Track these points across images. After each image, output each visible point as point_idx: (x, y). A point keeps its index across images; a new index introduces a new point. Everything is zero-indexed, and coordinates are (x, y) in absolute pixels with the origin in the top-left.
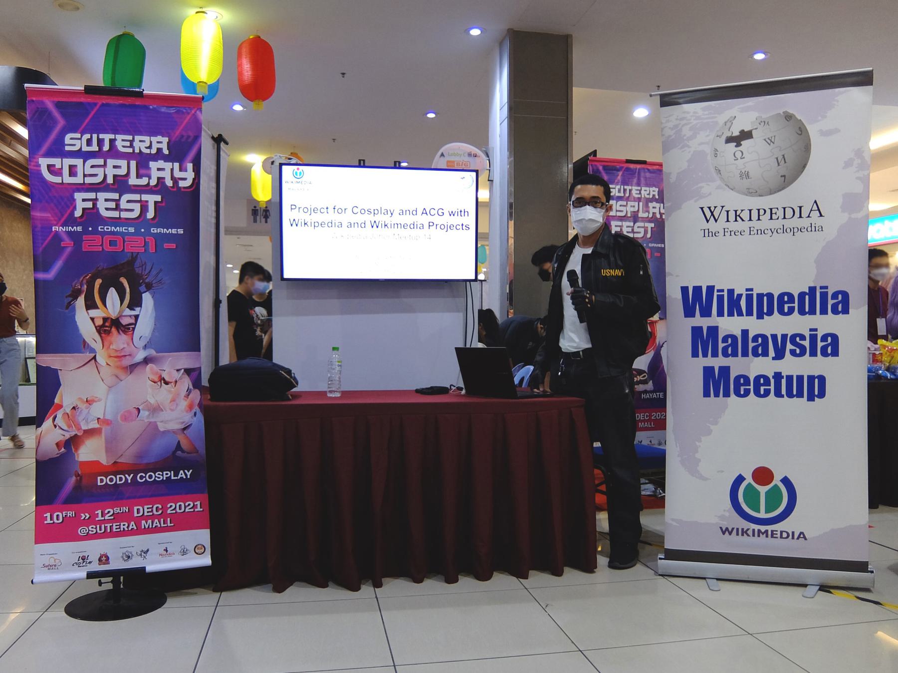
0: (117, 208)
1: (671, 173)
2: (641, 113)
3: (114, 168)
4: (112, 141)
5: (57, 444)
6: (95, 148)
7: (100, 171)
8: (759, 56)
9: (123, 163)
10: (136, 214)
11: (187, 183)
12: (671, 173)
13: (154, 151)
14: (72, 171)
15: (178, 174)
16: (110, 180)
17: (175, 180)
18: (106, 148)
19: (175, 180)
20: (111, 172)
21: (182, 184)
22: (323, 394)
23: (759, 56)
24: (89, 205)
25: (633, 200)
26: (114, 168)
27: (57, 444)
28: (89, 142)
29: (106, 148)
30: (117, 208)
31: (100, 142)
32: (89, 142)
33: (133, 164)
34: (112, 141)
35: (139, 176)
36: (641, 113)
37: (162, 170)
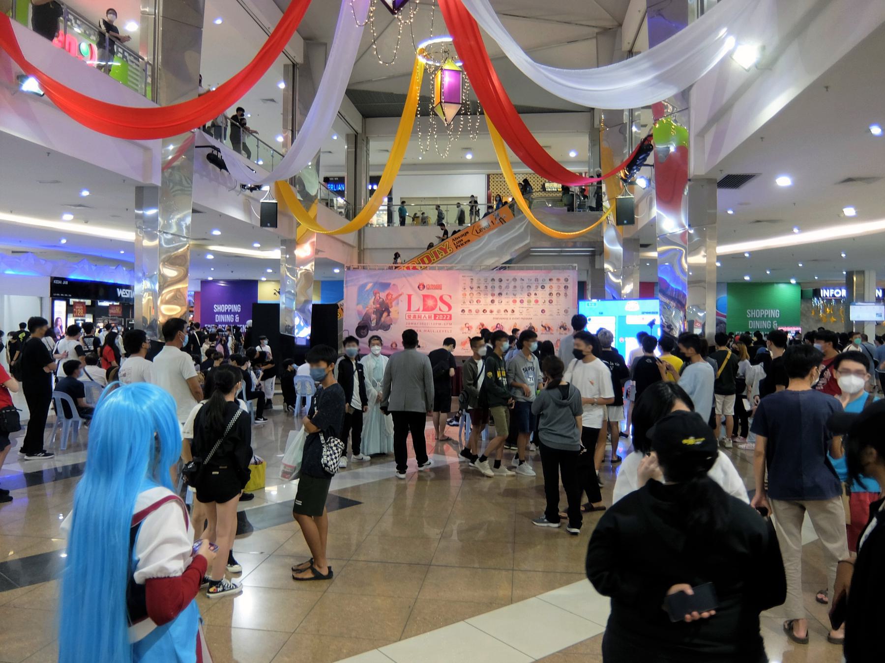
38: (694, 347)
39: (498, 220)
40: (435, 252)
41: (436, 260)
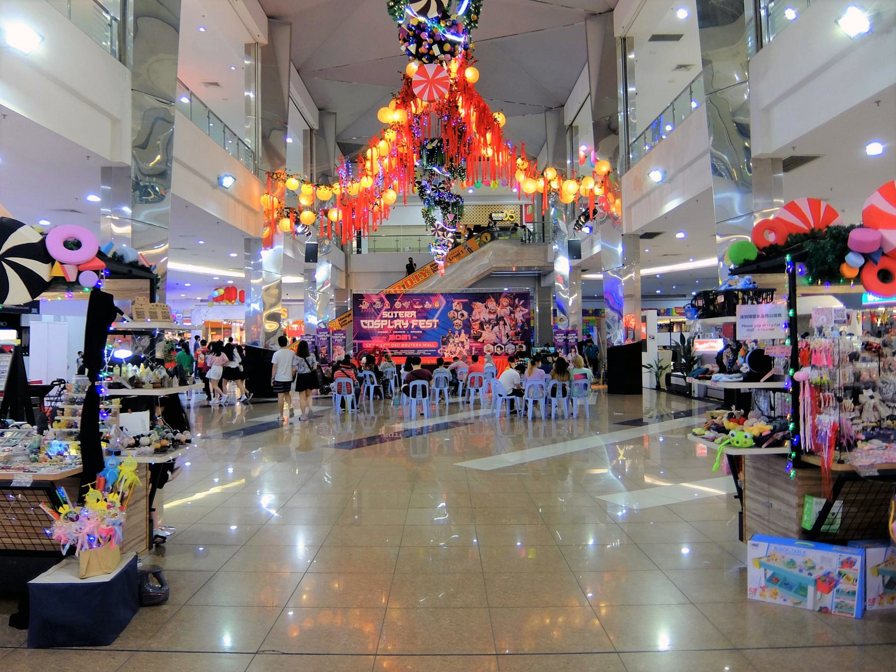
0: (425, 325)
1: (800, 584)
2: (93, 198)
3: (323, 335)
4: (398, 314)
5: (813, 308)
6: (392, 316)
7: (379, 324)
8: (680, 235)
9: (386, 321)
10: (431, 326)
11: (407, 327)
12: (800, 584)
13: (411, 316)
14: (371, 324)
15: (403, 324)
16: (382, 327)
17: (402, 326)
18: (396, 316)
19: (402, 326)
20: (383, 324)
21: (404, 327)
22: (41, 382)
23: (680, 235)
24: (416, 324)
25: (376, 410)
26: (323, 335)
27: (813, 308)
28: (390, 315)
29: (396, 316)
30: (425, 325)
31: (394, 314)
32: (390, 315)
33: (389, 321)
34: (398, 314)
35: (391, 325)
36: (93, 198)
37: (312, 340)
38: (114, 305)
39: (466, 249)
40: (416, 276)
41: (424, 278)
